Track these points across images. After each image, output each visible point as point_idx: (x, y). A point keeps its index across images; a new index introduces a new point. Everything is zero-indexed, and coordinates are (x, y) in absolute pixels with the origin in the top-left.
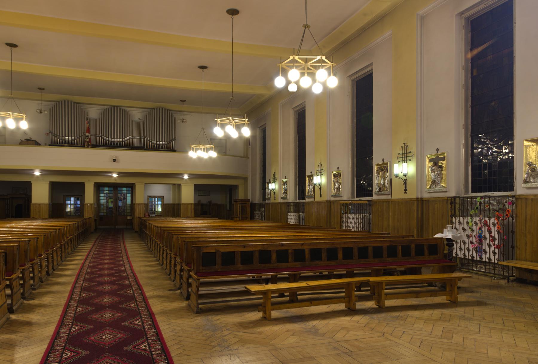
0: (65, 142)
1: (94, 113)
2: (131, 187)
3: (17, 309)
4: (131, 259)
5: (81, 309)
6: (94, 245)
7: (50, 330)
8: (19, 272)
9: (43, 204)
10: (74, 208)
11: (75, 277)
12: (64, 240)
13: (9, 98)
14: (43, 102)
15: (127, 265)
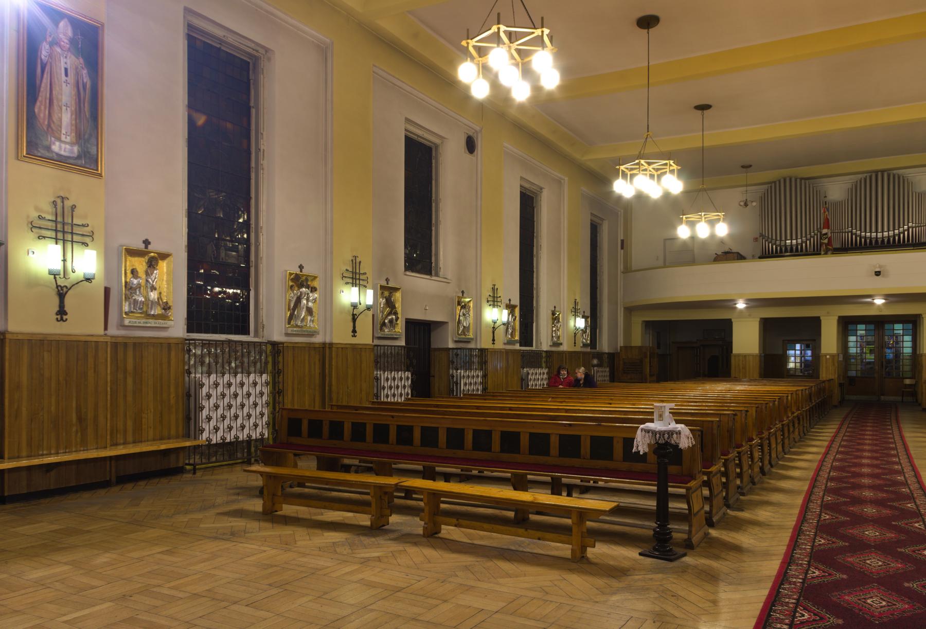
0: (786, 249)
1: (836, 191)
2: (913, 322)
3: (719, 521)
4: (917, 462)
5: (823, 541)
6: (839, 429)
7: (772, 567)
8: (721, 464)
9: (749, 355)
10: (801, 362)
11: (808, 483)
12: (788, 417)
13: (700, 190)
14: (749, 188)
15: (909, 474)
